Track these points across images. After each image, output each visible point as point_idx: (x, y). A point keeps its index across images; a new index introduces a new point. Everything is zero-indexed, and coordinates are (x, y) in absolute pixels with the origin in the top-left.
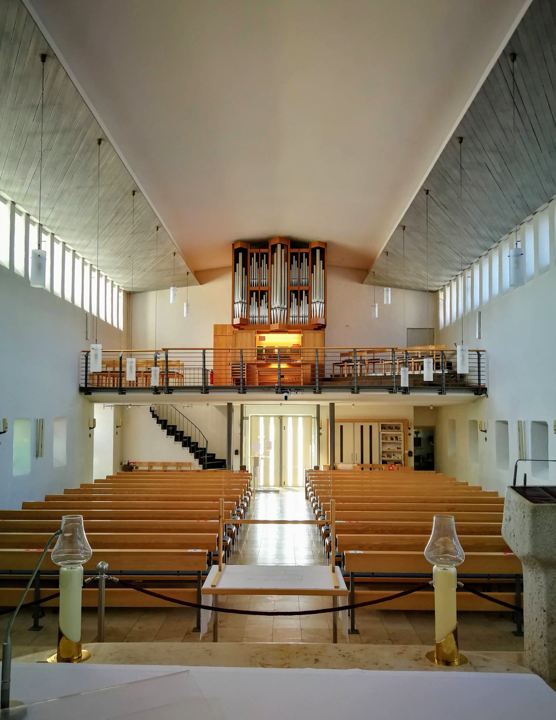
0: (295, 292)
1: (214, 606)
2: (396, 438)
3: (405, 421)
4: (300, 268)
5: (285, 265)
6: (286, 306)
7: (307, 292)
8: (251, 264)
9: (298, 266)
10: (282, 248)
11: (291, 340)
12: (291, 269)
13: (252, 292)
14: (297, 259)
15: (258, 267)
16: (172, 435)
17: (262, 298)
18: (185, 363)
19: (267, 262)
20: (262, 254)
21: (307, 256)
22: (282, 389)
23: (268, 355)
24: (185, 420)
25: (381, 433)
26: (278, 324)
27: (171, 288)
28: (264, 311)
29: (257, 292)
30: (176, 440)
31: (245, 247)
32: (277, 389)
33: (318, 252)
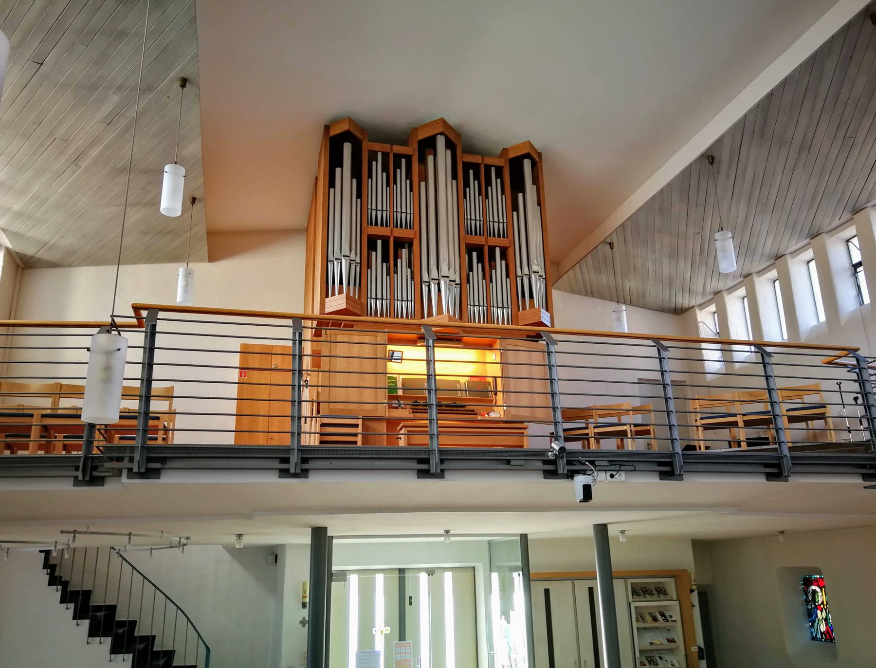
0: (479, 249)
2: (663, 615)
3: (677, 575)
4: (487, 197)
8: (370, 176)
9: (480, 194)
11: (458, 365)
12: (465, 197)
15: (388, 185)
16: (105, 635)
18: (179, 389)
19: (409, 176)
20: (398, 157)
21: (499, 175)
22: (569, 463)
23: (419, 398)
24: (171, 608)
25: (633, 605)
27: (167, 168)
29: (385, 241)
30: (115, 650)
31: (358, 134)
32: (554, 462)
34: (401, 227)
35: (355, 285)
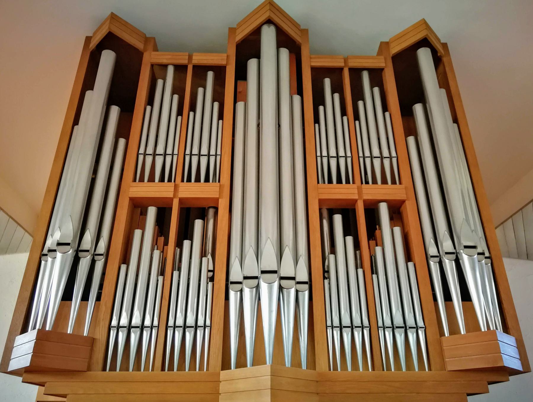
1: (76, 333)
4: (357, 117)
5: (292, 107)
6: (303, 276)
7: (397, 213)
8: (150, 101)
9: (344, 113)
10: (280, 44)
12: (317, 120)
13: (139, 207)
14: (337, 88)
15: (180, 112)
17: (186, 233)
19: (218, 96)
26: (265, 369)
28: (191, 309)
29: (180, 69)
33: (424, 57)
34: (198, 180)
35: (85, 297)
